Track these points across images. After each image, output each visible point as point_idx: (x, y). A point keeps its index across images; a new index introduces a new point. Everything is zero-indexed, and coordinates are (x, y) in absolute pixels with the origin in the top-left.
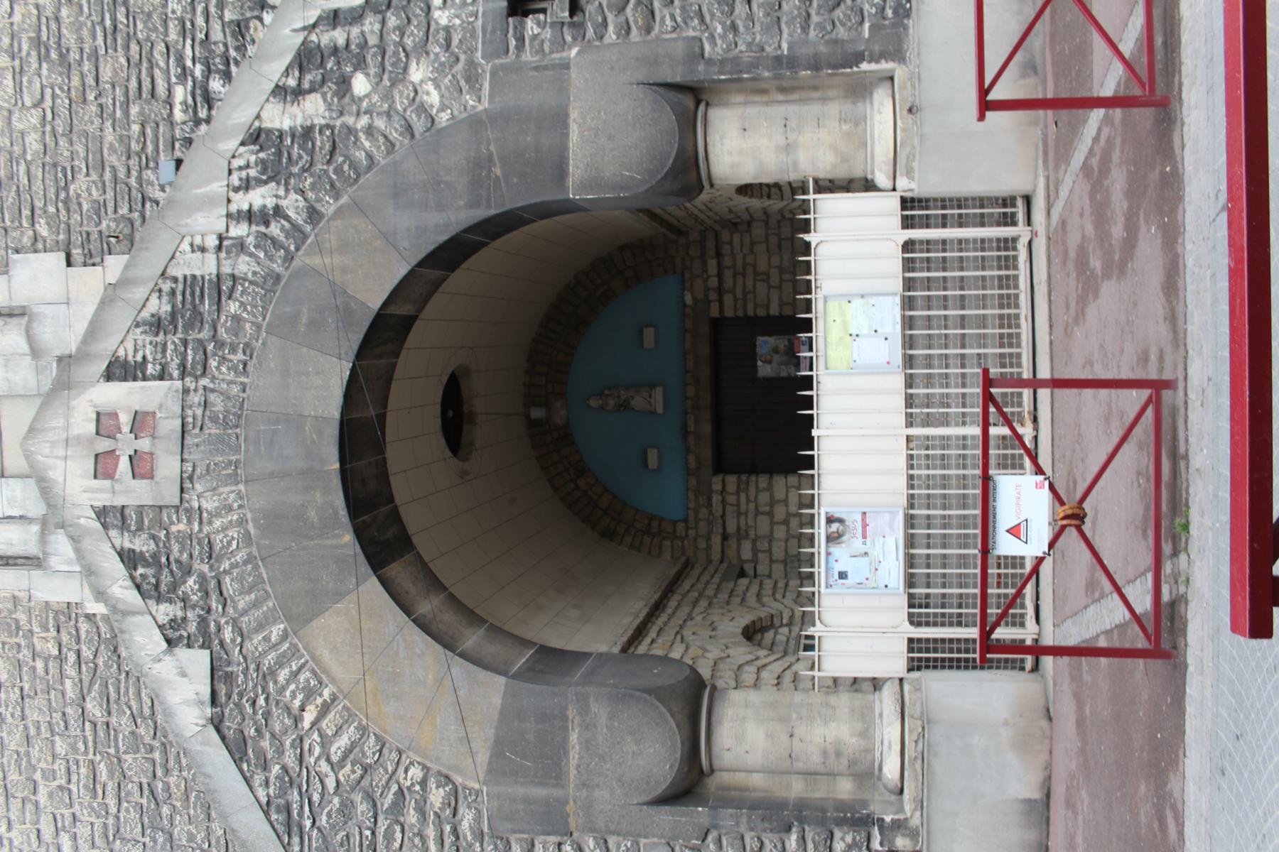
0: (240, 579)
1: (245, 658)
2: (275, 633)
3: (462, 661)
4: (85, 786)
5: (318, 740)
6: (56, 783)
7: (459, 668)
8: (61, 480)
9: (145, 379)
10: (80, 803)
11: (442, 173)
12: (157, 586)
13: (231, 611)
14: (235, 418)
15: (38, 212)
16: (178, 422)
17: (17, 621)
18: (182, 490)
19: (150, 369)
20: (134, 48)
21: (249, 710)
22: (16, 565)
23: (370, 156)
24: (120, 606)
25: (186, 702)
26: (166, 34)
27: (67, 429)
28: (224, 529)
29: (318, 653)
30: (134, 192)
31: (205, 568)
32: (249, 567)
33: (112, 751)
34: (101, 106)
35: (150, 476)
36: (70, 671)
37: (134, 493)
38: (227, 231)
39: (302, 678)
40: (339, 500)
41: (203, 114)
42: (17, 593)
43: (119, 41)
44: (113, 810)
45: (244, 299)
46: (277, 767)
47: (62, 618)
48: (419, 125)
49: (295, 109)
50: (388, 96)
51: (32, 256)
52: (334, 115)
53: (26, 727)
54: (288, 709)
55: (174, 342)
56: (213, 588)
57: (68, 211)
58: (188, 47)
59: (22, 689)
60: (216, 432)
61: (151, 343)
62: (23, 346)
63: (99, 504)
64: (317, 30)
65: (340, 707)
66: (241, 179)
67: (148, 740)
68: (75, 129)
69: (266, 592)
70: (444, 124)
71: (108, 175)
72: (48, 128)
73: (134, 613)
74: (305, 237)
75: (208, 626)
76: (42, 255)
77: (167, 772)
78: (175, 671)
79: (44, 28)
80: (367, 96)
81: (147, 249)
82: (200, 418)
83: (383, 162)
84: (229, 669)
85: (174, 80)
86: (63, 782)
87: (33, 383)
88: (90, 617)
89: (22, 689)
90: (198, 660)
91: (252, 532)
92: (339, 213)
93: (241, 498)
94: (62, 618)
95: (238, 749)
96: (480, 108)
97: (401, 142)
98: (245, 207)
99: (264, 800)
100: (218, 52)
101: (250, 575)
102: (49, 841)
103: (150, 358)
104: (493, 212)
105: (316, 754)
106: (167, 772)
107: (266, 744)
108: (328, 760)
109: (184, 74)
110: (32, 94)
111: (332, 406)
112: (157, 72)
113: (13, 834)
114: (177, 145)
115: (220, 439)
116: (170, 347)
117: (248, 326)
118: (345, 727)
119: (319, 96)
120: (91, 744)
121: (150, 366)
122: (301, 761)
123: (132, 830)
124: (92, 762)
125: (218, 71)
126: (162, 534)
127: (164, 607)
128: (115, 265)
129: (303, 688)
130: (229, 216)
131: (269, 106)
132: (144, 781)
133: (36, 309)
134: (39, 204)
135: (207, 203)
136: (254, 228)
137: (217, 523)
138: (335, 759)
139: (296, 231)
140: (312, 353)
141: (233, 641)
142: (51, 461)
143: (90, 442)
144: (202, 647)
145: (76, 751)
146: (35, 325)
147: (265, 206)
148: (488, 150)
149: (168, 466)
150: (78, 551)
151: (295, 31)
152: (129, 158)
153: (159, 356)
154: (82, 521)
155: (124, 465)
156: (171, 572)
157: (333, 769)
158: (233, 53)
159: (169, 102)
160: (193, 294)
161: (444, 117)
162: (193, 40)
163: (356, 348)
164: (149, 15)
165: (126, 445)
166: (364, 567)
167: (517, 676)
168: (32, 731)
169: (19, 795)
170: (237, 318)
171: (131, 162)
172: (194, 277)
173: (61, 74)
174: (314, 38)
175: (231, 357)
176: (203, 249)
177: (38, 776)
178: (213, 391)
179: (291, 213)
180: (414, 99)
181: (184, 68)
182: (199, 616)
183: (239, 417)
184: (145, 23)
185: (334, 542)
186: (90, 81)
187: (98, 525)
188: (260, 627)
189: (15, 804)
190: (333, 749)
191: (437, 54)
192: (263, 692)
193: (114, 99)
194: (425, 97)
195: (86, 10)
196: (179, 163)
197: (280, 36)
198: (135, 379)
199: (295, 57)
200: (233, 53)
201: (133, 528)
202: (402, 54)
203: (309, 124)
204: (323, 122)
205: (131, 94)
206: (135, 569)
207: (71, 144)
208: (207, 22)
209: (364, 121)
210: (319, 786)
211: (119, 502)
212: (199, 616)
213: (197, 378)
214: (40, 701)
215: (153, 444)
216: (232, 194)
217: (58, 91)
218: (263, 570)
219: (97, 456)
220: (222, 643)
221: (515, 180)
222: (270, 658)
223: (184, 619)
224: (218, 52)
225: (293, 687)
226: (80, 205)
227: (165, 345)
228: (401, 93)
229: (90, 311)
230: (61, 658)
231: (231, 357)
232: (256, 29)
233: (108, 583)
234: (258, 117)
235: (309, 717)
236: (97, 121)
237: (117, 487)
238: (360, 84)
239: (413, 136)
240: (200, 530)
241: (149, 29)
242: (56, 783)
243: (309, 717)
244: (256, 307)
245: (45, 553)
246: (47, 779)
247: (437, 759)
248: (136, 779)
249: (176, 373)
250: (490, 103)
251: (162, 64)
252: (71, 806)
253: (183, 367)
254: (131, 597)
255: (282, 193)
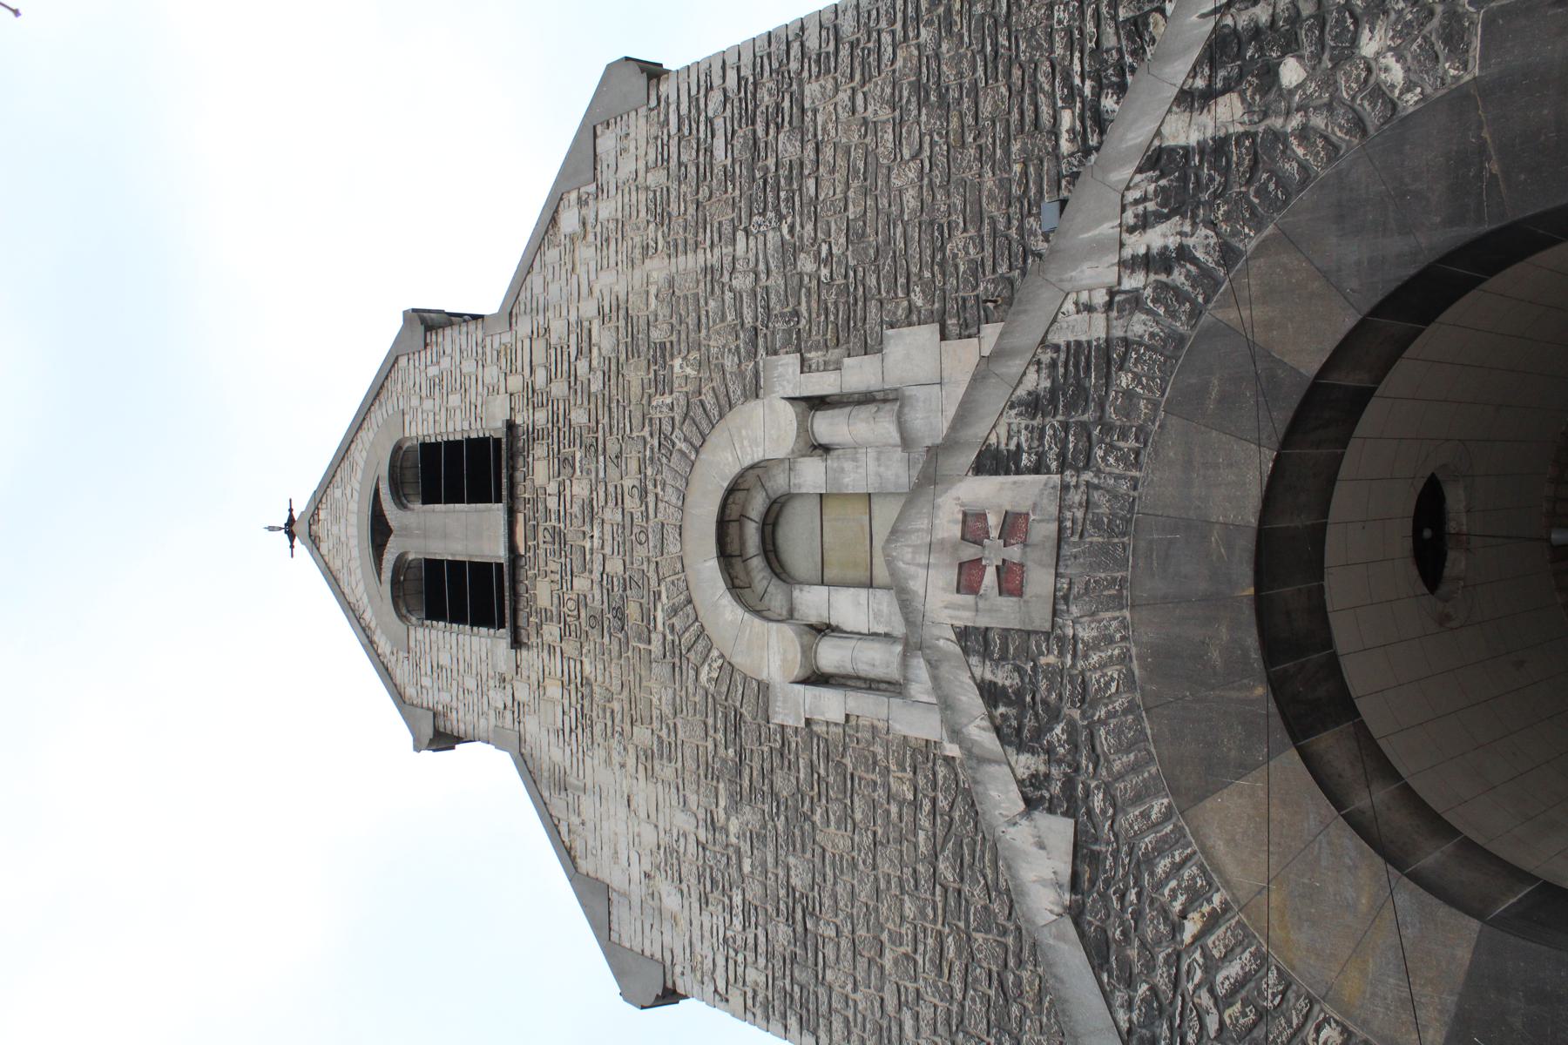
0: (1118, 732)
1: (1116, 836)
2: (1156, 809)
3: (1412, 885)
4: (931, 960)
5: (1201, 961)
6: (902, 949)
7: (1408, 896)
8: (921, 592)
9: (1018, 472)
10: (925, 979)
11: (1407, 180)
12: (1019, 730)
13: (1104, 773)
14: (1124, 522)
15: (914, 279)
16: (1054, 527)
17: (874, 755)
18: (1055, 613)
19: (1025, 460)
20: (1017, 73)
21: (1116, 905)
22: (878, 690)
23: (1303, 167)
24: (976, 750)
25: (1042, 882)
26: (1052, 51)
27: (931, 531)
28: (1103, 666)
29: (1209, 843)
30: (1014, 245)
31: (1076, 714)
32: (1130, 717)
33: (962, 925)
34: (980, 147)
35: (1018, 592)
36: (925, 822)
37: (1000, 613)
38: (1119, 283)
39: (1186, 874)
40: (1251, 640)
41: (1093, 141)
42: (876, 722)
43: (1000, 68)
44: (959, 996)
45: (1138, 370)
46: (1145, 987)
47: (920, 758)
48: (1373, 115)
49: (1205, 118)
50: (1329, 82)
51: (905, 330)
52: (1256, 119)
53: (876, 879)
54: (1164, 912)
55: (1053, 426)
56: (1083, 740)
57: (944, 275)
58: (1076, 61)
59: (875, 833)
60: (1104, 543)
61: (1026, 428)
62: (895, 437)
63: (960, 624)
64: (1233, 10)
65: (1233, 922)
66: (1136, 216)
67: (1001, 920)
68: (953, 178)
69: (1149, 753)
70: (1411, 110)
71: (986, 228)
72: (926, 181)
73: (990, 761)
74: (1218, 284)
75: (1075, 789)
76: (916, 327)
77: (1020, 963)
78: (1032, 840)
79: (924, 69)
80: (1300, 86)
81: (1025, 311)
82: (1080, 522)
83: (1322, 174)
84: (1096, 848)
85: (1060, 104)
86: (910, 950)
87: (904, 480)
88: (949, 761)
89: (875, 833)
90: (1060, 830)
91: (1137, 672)
92: (1261, 248)
93: (1126, 628)
94: (920, 758)
95: (1098, 952)
96: (1467, 78)
97: (1348, 143)
98: (1142, 251)
99: (1125, 1026)
100: (1111, 61)
101: (1130, 729)
102: (892, 1014)
103: (1025, 446)
104: (1486, 228)
105: (1196, 980)
106: (1020, 963)
107: (1133, 953)
108: (1212, 991)
109: (1069, 101)
110: (910, 145)
111: (1249, 514)
112: (1041, 98)
113: (859, 996)
114: (1064, 183)
115: (1103, 550)
116: (1049, 432)
117: (1142, 403)
118: (1238, 950)
119: (1235, 96)
120: (940, 912)
121: (1025, 456)
122: (1175, 983)
123: (976, 1024)
124: (940, 933)
125: (1111, 85)
126: (1029, 667)
127: (1025, 758)
128: (991, 332)
129: (1187, 889)
130: (1122, 264)
131: (1171, 118)
132: (994, 968)
133: (909, 392)
134: (915, 270)
135: (1097, 248)
136: (1152, 277)
137: (1095, 658)
138: (1221, 991)
139: (1205, 278)
140: (1224, 438)
141: (1104, 812)
142: (912, 569)
143: (955, 547)
144: (1065, 814)
145: (924, 916)
146: (906, 410)
147: (1166, 248)
148: (1479, 137)
149: (1040, 581)
150: (935, 679)
151: (1203, 16)
152: (1009, 205)
153: (1036, 443)
154: (941, 642)
155: (990, 577)
156: (1036, 715)
157: (1216, 1004)
158: (1128, 59)
159: (1055, 132)
160: (1077, 366)
161: (1412, 98)
162: (1082, 52)
163: (1282, 429)
164: (1033, 32)
165: (994, 553)
166: (1280, 734)
167: (1500, 923)
168: (883, 885)
169: (865, 953)
170: (1128, 394)
171: (1012, 210)
172: (1079, 343)
173: (939, 118)
174: (1229, 21)
175: (1121, 444)
176: (1089, 308)
177: (885, 937)
178: (1097, 487)
179: (1200, 254)
180: (1366, 80)
181: (1071, 88)
182: (1065, 774)
183: (1129, 521)
184: (1028, 41)
185: (1242, 695)
186: (969, 120)
187: (958, 649)
188: (1138, 798)
189: (862, 963)
190: (1219, 978)
191: (1400, 12)
192: (1136, 884)
193: (994, 138)
194: (1383, 76)
195: (966, 39)
196: (1063, 203)
197: (1188, 25)
198: (1007, 473)
199: (1205, 50)
200: (1128, 59)
201: (996, 656)
202: (1349, 21)
203: (1222, 133)
204: (1241, 129)
205: (1013, 127)
206: (996, 707)
207: (949, 197)
208: (1098, 26)
209: (1296, 120)
210: (1196, 1023)
211: (982, 622)
212: (1065, 774)
213: (1078, 471)
214: (892, 850)
215: (1024, 553)
216: (1125, 236)
217: (936, 138)
218: (1146, 724)
219: (961, 565)
220: (1090, 812)
221: (1523, 177)
222: (1149, 839)
223: (1047, 776)
224: (1111, 61)
225: (1173, 884)
226: (956, 267)
227: (1042, 430)
228: (1348, 75)
229: (960, 391)
230: (916, 805)
231: (1121, 444)
232: (1156, 25)
233: (965, 721)
234: (1158, 133)
235: (1191, 927)
236: (976, 166)
237: (981, 604)
238: (1291, 72)
239: (1364, 132)
240: (1074, 665)
241: (1033, 48)
242: (902, 949)
243: (1191, 927)
244: (1153, 379)
245: (906, 678)
246: (894, 943)
247: (1365, 1024)
248: (985, 965)
249: (1054, 465)
250: (1481, 69)
251: (1047, 87)
252: (916, 980)
253: (1062, 456)
254: (987, 740)
255: (1187, 228)
